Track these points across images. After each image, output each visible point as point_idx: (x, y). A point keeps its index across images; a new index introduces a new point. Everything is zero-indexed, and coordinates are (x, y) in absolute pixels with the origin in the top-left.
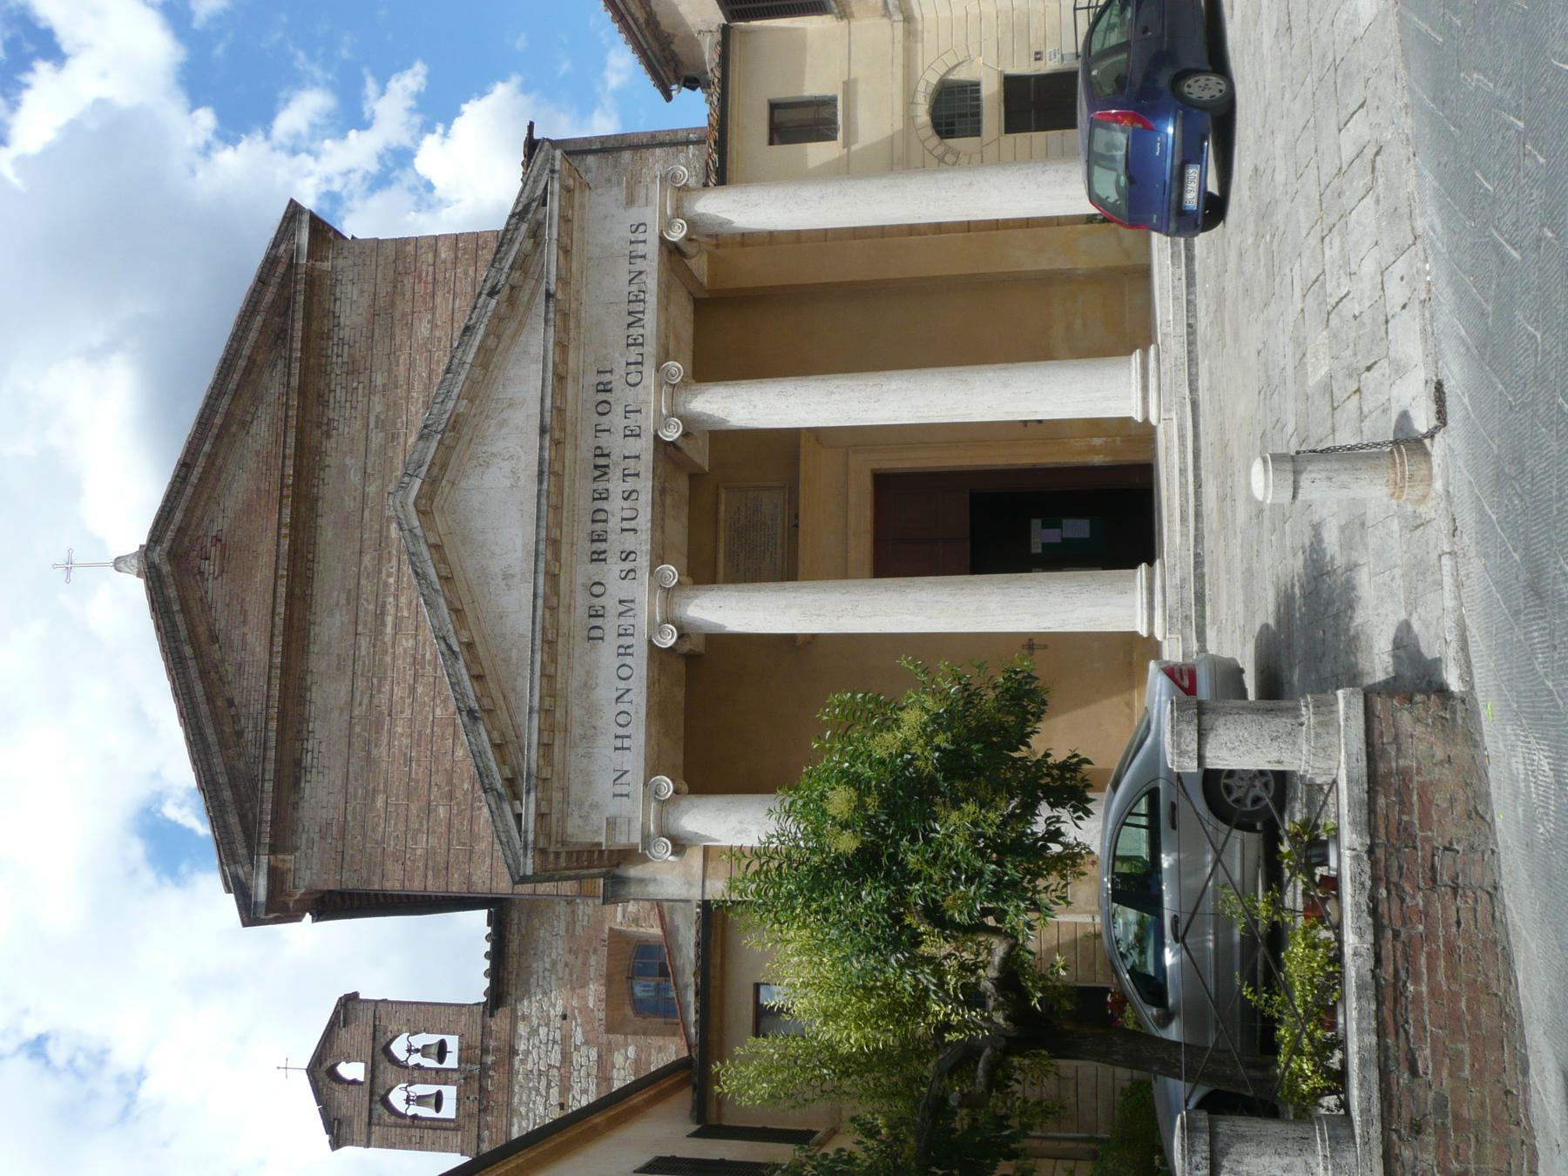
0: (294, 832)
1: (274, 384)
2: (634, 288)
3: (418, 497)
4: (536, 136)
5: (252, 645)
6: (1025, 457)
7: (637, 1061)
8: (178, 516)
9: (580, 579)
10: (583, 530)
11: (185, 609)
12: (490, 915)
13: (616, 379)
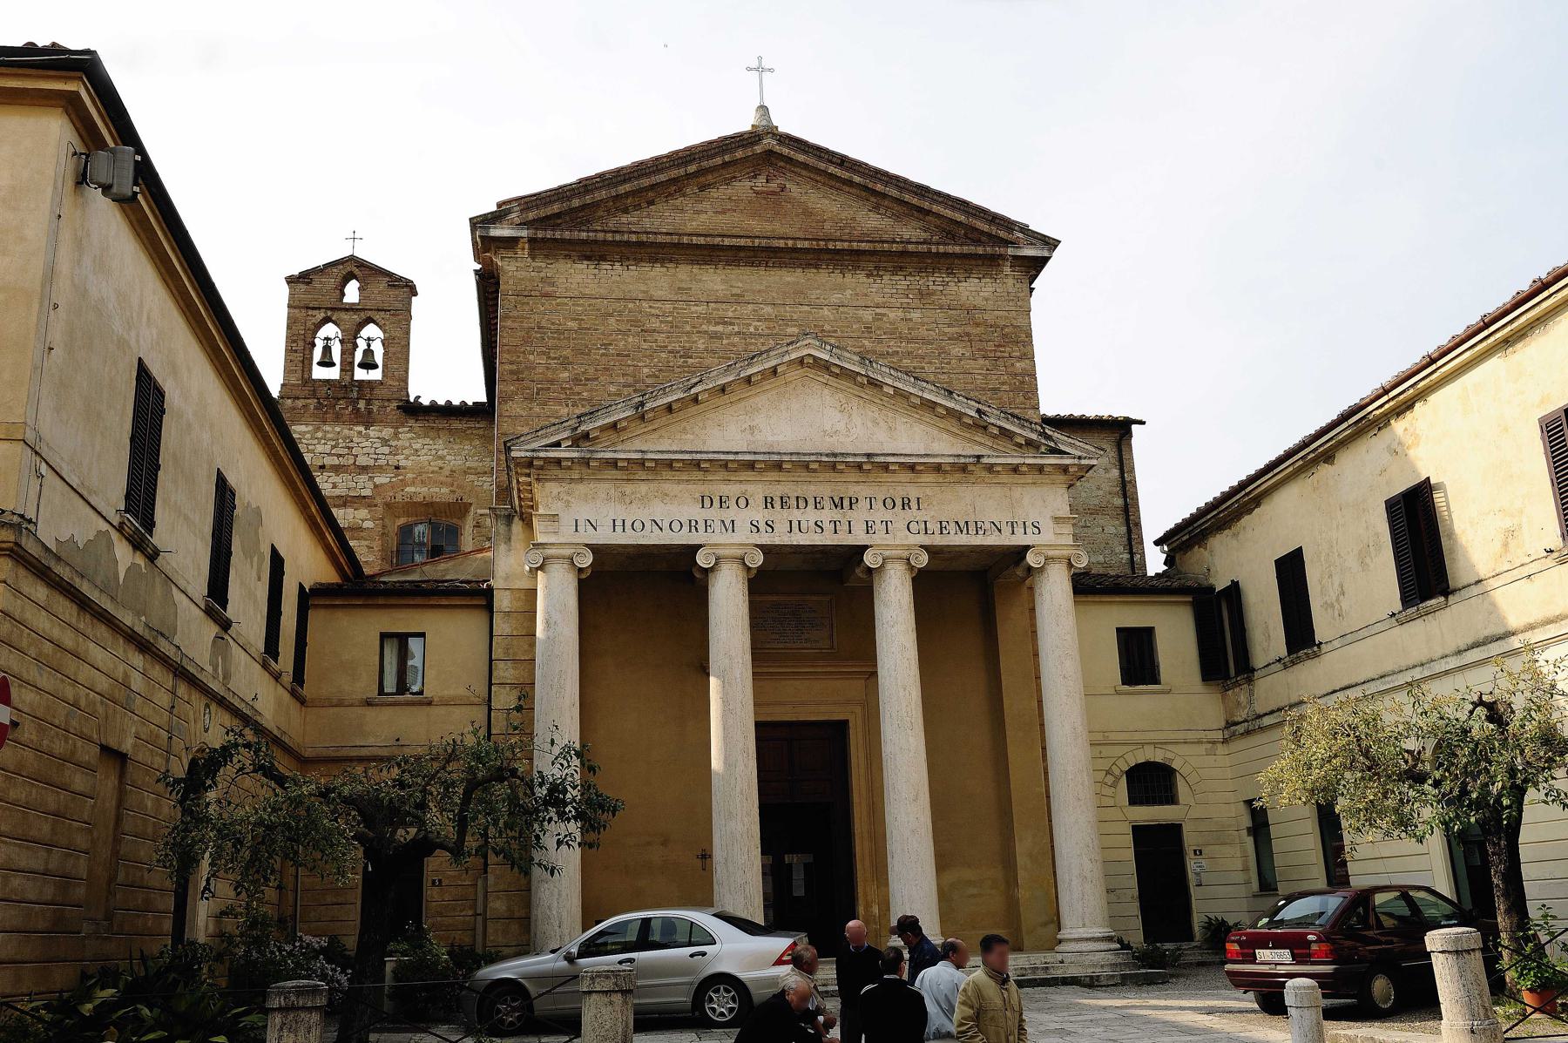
0: (547, 256)
1: (910, 231)
2: (987, 526)
3: (815, 358)
4: (1134, 427)
5: (694, 216)
6: (861, 847)
7: (360, 529)
8: (801, 157)
9: (750, 488)
10: (791, 490)
11: (725, 165)
12: (482, 404)
13: (913, 514)
